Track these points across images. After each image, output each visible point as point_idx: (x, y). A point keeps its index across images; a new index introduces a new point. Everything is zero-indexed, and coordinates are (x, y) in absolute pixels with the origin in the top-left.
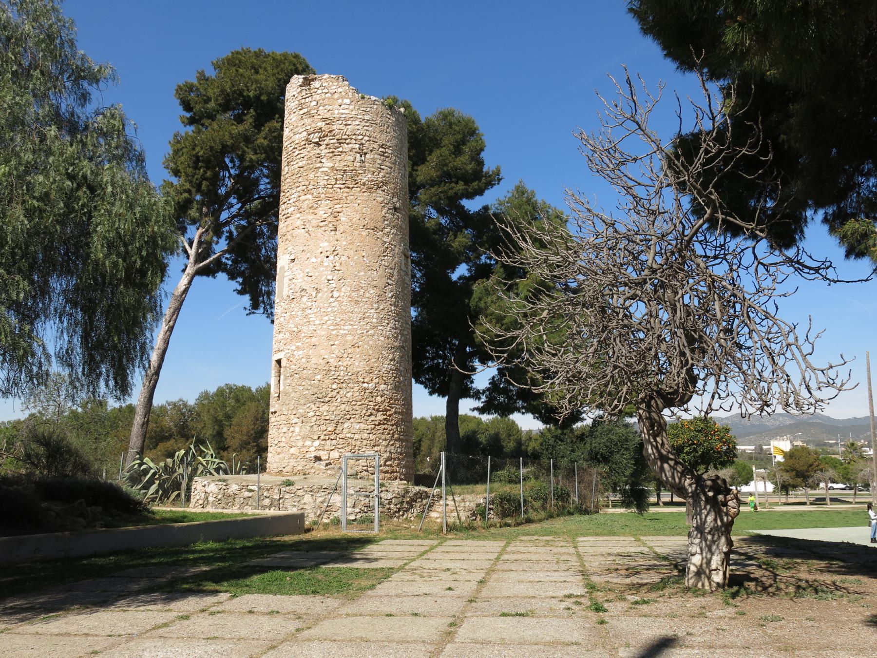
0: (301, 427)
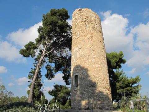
0: (87, 94)
